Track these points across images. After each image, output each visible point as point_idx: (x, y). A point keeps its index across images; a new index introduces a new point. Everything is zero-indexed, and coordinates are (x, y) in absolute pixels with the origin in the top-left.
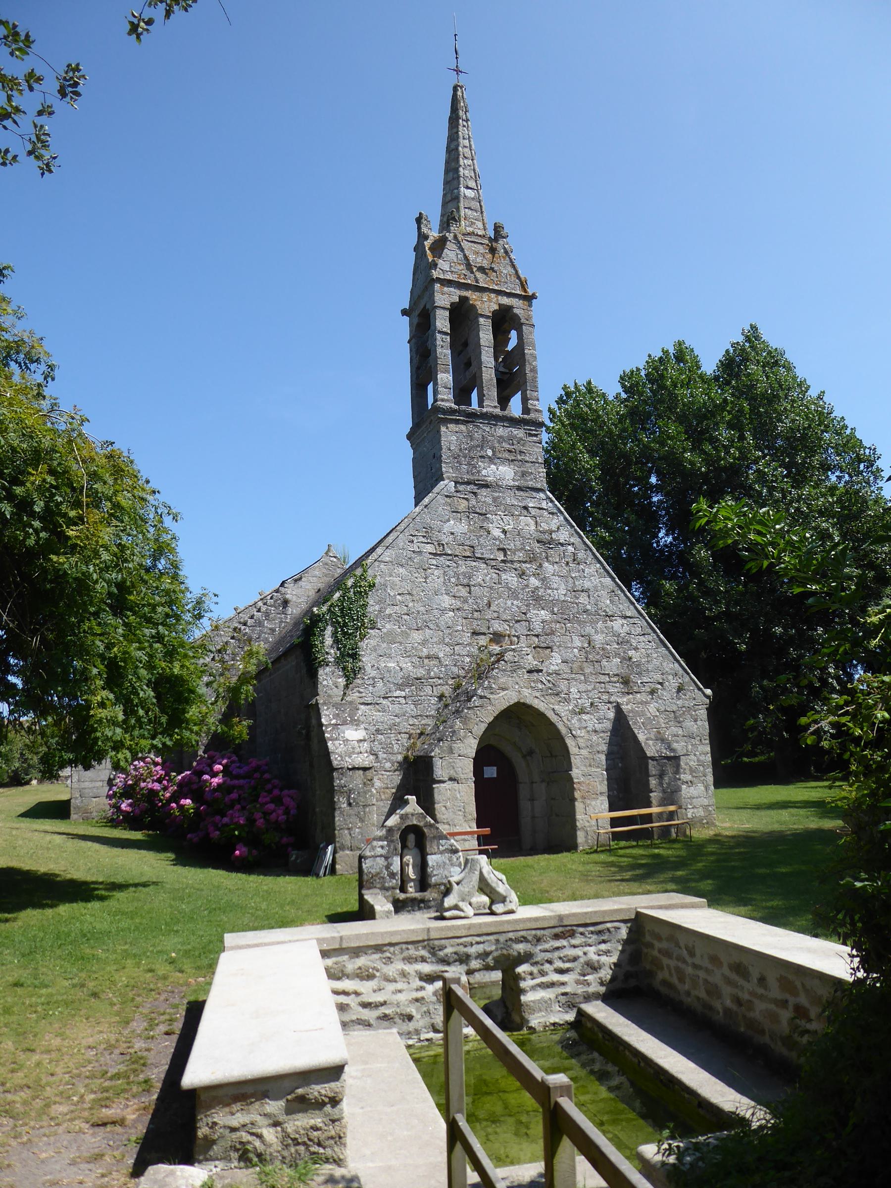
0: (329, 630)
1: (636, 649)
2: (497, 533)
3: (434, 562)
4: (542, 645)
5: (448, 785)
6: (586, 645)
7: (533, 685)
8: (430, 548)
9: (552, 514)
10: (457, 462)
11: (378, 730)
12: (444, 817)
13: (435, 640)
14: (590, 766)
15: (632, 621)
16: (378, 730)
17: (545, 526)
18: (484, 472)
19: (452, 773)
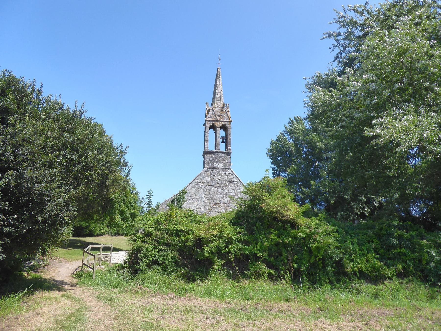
0: (176, 202)
2: (217, 180)
18: (215, 165)
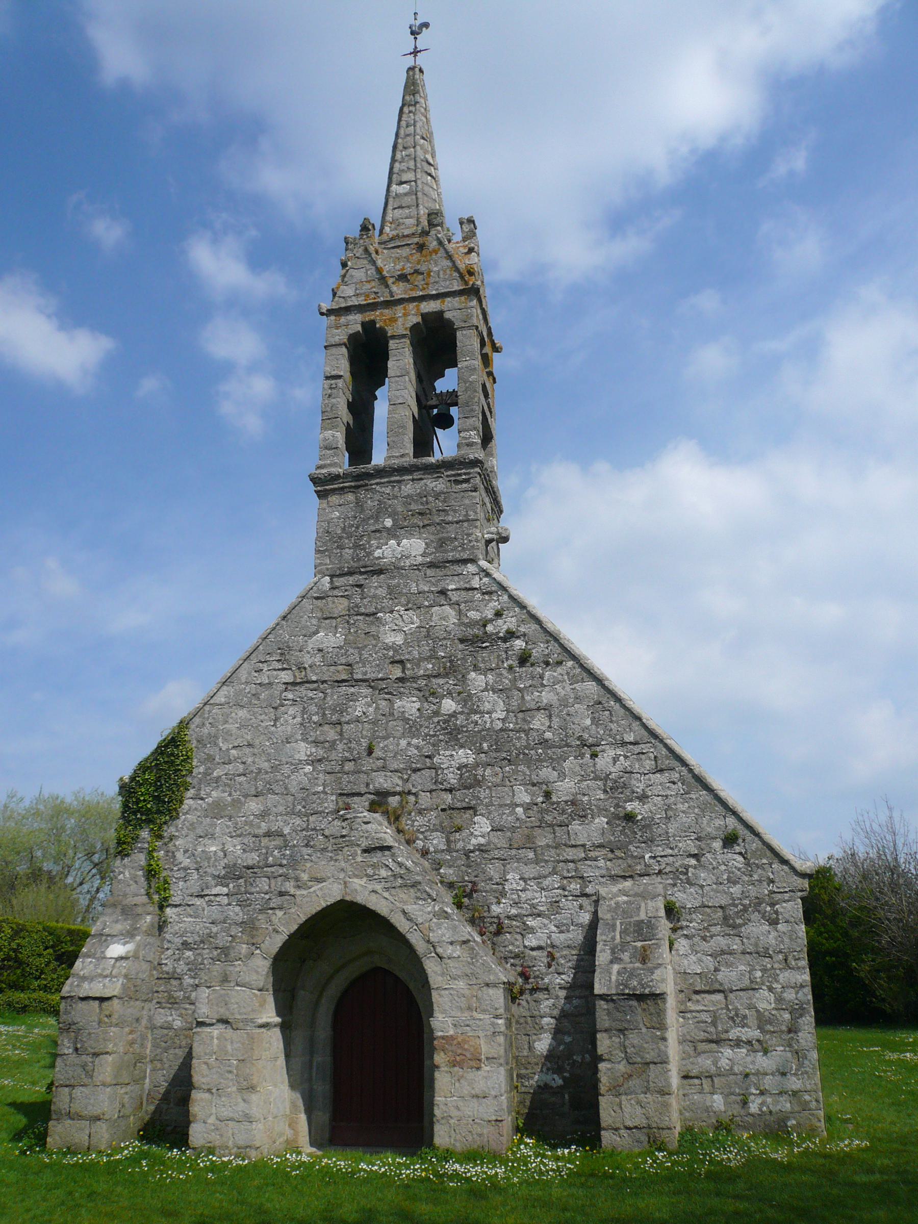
1: (643, 798)
3: (290, 696)
4: (459, 805)
5: (216, 1031)
6: (540, 799)
7: (370, 871)
8: (286, 677)
9: (490, 593)
10: (338, 547)
11: (185, 944)
12: (203, 1080)
13: (281, 809)
14: (469, 1008)
15: (637, 749)
16: (185, 944)
17: (473, 615)
19: (223, 1012)
